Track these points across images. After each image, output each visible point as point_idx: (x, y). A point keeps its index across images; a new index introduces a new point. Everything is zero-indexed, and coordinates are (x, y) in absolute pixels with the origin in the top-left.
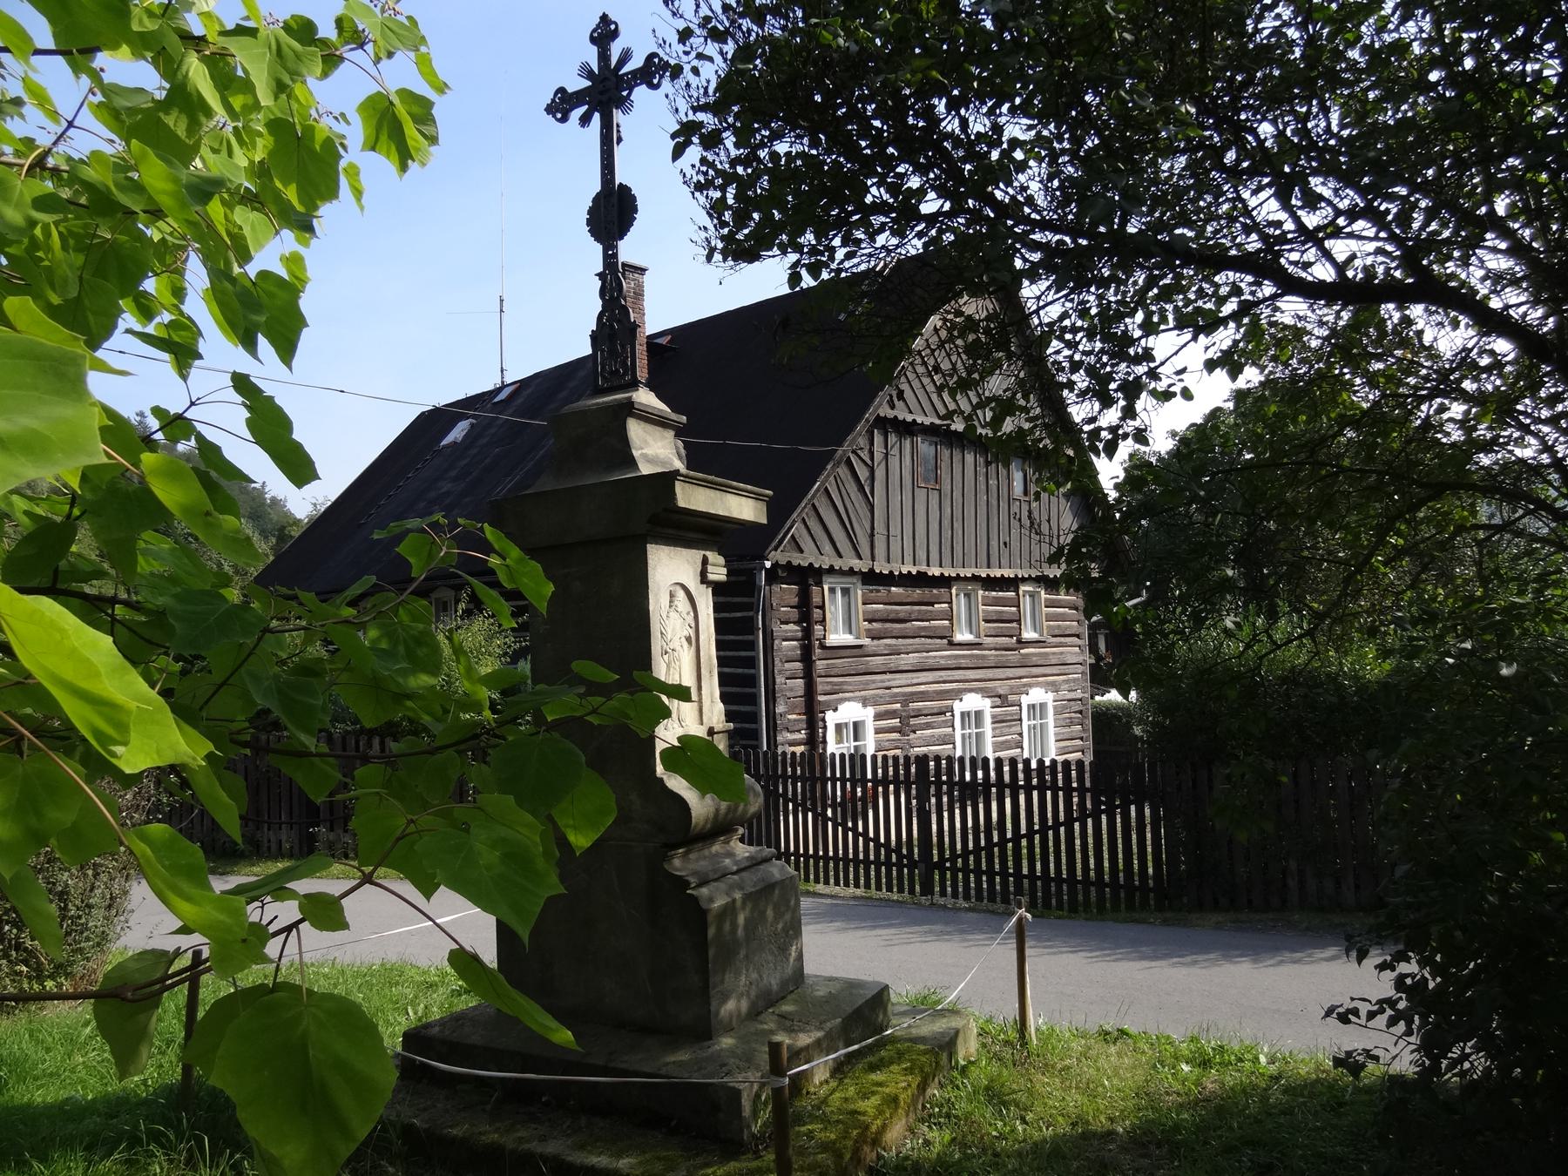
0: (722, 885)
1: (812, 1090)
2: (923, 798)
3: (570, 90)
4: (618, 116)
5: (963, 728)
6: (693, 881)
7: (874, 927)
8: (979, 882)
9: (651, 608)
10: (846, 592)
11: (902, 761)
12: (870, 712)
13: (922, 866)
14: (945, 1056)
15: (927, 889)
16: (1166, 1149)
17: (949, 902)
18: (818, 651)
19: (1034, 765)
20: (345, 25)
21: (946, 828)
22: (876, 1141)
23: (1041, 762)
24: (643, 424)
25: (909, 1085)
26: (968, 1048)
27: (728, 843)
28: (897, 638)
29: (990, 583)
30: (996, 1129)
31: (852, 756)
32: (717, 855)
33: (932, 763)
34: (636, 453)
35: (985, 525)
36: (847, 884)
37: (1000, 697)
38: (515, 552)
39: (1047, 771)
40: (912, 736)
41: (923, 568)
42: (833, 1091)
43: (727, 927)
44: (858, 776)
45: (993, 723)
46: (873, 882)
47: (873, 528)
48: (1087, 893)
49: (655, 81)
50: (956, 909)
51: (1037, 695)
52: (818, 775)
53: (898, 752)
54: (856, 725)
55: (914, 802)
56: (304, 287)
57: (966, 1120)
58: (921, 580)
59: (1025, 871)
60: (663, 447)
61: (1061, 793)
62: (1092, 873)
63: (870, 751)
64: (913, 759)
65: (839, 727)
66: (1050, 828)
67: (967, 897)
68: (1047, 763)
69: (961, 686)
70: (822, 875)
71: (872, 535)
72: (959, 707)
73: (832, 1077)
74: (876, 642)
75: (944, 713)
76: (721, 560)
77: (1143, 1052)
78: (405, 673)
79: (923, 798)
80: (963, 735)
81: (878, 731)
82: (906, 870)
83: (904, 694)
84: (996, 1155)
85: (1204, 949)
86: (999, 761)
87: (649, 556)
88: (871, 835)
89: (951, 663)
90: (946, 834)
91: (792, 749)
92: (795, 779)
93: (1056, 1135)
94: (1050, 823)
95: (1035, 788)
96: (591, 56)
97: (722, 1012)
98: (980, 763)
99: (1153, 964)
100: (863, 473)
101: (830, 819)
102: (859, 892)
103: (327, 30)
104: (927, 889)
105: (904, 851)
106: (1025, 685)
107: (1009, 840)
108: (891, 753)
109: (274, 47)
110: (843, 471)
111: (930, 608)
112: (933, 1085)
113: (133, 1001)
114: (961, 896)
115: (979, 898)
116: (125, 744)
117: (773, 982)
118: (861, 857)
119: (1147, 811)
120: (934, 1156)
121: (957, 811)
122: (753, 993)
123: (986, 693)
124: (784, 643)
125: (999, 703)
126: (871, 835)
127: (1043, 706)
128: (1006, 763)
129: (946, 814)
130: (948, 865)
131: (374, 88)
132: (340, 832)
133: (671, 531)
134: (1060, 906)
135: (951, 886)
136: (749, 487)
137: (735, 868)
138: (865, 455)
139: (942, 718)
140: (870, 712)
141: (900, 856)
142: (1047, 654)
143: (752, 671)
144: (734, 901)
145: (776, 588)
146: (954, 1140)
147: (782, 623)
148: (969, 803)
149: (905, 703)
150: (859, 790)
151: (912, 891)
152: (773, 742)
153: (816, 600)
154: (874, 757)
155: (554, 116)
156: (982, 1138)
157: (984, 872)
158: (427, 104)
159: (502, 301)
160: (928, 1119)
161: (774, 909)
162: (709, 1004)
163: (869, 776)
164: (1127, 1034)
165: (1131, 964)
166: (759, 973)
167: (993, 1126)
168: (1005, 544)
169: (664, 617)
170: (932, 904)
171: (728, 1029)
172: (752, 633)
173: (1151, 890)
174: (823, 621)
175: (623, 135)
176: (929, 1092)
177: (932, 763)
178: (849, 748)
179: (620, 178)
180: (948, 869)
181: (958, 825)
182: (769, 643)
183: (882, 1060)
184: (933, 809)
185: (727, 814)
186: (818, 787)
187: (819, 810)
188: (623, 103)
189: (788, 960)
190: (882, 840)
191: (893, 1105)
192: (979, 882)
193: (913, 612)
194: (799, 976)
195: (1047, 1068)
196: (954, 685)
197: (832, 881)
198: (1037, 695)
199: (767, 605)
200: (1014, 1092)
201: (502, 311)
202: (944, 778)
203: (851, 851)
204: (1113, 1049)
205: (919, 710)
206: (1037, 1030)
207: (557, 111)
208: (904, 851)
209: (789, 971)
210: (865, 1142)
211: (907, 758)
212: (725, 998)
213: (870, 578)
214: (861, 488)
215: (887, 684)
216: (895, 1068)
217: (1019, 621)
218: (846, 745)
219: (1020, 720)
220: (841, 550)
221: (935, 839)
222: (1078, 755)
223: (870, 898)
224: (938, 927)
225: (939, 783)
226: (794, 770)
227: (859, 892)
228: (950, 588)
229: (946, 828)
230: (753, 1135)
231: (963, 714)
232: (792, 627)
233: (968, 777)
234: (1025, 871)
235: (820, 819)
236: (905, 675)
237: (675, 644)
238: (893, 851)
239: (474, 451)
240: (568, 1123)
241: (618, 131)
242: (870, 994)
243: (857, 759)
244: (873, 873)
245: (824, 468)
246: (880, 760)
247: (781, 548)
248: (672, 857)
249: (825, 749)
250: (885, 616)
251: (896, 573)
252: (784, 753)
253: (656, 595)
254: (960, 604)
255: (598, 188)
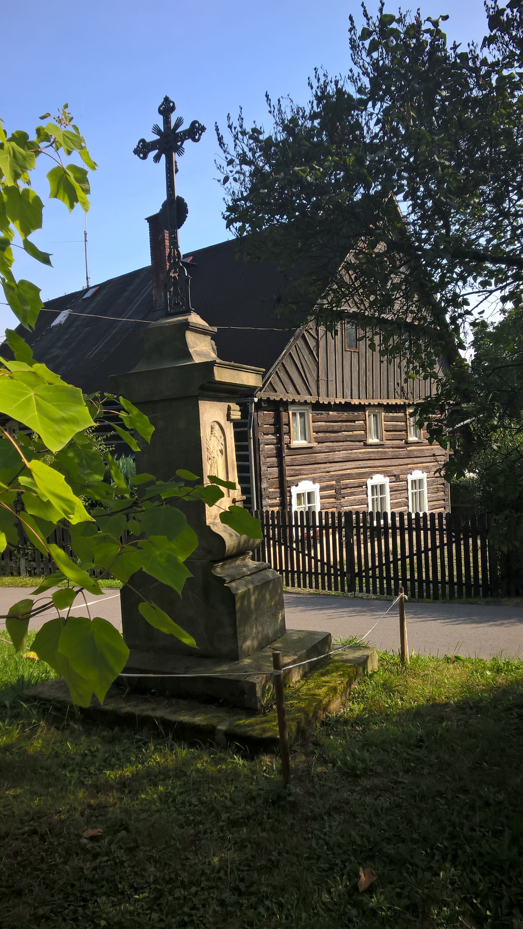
0: (242, 581)
1: (292, 685)
2: (349, 536)
3: (148, 140)
4: (176, 157)
5: (373, 495)
6: (228, 579)
7: (322, 609)
8: (381, 584)
9: (202, 435)
10: (302, 415)
11: (336, 515)
12: (317, 486)
13: (349, 575)
14: (361, 669)
15: (352, 588)
16: (474, 710)
17: (364, 595)
18: (286, 451)
19: (413, 516)
20: (41, 132)
21: (363, 553)
22: (325, 709)
23: (417, 514)
24: (194, 334)
25: (342, 682)
26: (373, 665)
27: (244, 560)
28: (333, 442)
29: (389, 408)
30: (387, 703)
31: (307, 513)
32: (239, 566)
33: (354, 516)
34: (191, 350)
35: (385, 374)
36: (305, 586)
37: (395, 476)
38: (135, 411)
39: (422, 520)
40: (343, 500)
41: (348, 400)
42: (303, 685)
43: (246, 603)
44: (311, 524)
45: (391, 491)
46: (320, 585)
47: (318, 376)
48: (444, 588)
49: (197, 137)
50: (368, 599)
51: (417, 475)
52: (287, 524)
53: (334, 510)
54: (309, 494)
55: (344, 539)
56: (11, 264)
57: (372, 700)
58: (347, 407)
59: (408, 577)
60: (205, 346)
61: (429, 532)
62: (447, 578)
63: (318, 510)
64: (343, 514)
65: (299, 496)
66: (423, 552)
67: (375, 592)
68: (421, 515)
69: (371, 470)
70: (290, 581)
71: (318, 381)
72: (370, 482)
73: (301, 679)
74: (321, 445)
75: (362, 486)
76: (238, 408)
77: (468, 667)
78: (90, 474)
79: (349, 536)
80: (373, 499)
81: (322, 498)
82: (339, 578)
83: (337, 475)
84: (387, 715)
85: (508, 616)
86: (393, 514)
87: (200, 407)
88: (319, 558)
89: (366, 456)
90: (363, 557)
91: (272, 509)
92: (274, 526)
93: (419, 705)
94: (423, 549)
95: (414, 529)
96: (159, 121)
97: (244, 646)
98: (382, 516)
99: (479, 625)
100: (312, 343)
101: (295, 549)
102: (312, 591)
103: (33, 137)
104: (352, 588)
105: (338, 567)
106: (410, 469)
107: (399, 560)
108: (330, 510)
109: (12, 153)
110: (300, 343)
111: (353, 424)
112: (354, 683)
113: (22, 620)
114: (371, 592)
115: (382, 593)
116: (73, 514)
117: (269, 632)
118: (313, 571)
119: (479, 542)
120: (355, 716)
121: (369, 544)
122: (260, 637)
123: (386, 474)
124: (266, 446)
125: (394, 480)
126: (319, 558)
127: (421, 481)
128: (397, 515)
129: (362, 546)
130: (364, 574)
131: (55, 165)
132: (8, 560)
133: (211, 393)
134: (428, 596)
135: (366, 586)
136: (253, 367)
137: (249, 573)
138: (313, 333)
139: (360, 489)
140: (317, 486)
141: (336, 570)
142: (423, 450)
143: (247, 463)
144: (249, 589)
145: (260, 413)
146: (364, 709)
147: (265, 434)
148: (376, 539)
149: (338, 481)
150: (311, 532)
151: (343, 590)
152: (260, 505)
153: (285, 420)
154: (320, 513)
155: (139, 156)
156: (380, 707)
157: (384, 578)
158: (85, 173)
159: (86, 234)
160: (352, 699)
161: (270, 594)
162: (237, 643)
163: (318, 524)
164: (460, 659)
165: (466, 625)
166: (262, 627)
167: (385, 701)
168: (398, 384)
169: (208, 439)
170: (355, 597)
171: (248, 656)
172: (247, 441)
173: (480, 586)
174: (289, 433)
175: (178, 168)
176: (353, 686)
177: (354, 516)
178: (305, 508)
179: (178, 193)
180: (364, 576)
181: (369, 552)
182: (257, 446)
183: (328, 671)
184: (355, 543)
185: (244, 544)
186: (288, 530)
187: (288, 544)
188: (179, 150)
189: (277, 621)
190: (325, 561)
191: (333, 692)
192: (381, 584)
193: (343, 426)
194: (283, 628)
195: (416, 675)
196: (367, 470)
197: (296, 585)
198: (417, 475)
199: (256, 424)
200: (397, 686)
201: (86, 240)
202: (361, 525)
203: (307, 568)
204: (451, 666)
205: (347, 484)
206: (411, 657)
207: (140, 153)
208: (338, 567)
209: (278, 627)
210: (320, 708)
211: (340, 513)
212: (245, 639)
213: (317, 407)
214: (311, 352)
215: (327, 470)
216: (334, 674)
217: (406, 431)
218: (304, 506)
219: (407, 489)
220: (299, 390)
221: (356, 560)
222: (439, 510)
223: (319, 594)
224: (358, 608)
225: (358, 528)
226: (273, 522)
227: (312, 591)
228: (365, 411)
229: (363, 553)
230: (262, 706)
231: (372, 487)
232: (270, 436)
233: (375, 524)
234: (408, 577)
235: (289, 549)
236: (338, 464)
237: (215, 454)
238: (332, 567)
239: (72, 329)
240: (166, 703)
241: (176, 166)
242: (321, 638)
243: (310, 513)
244: (320, 580)
245: (288, 341)
246: (323, 515)
247: (264, 390)
248: (216, 567)
249: (291, 509)
250: (326, 429)
251: (333, 403)
252: (267, 512)
253: (204, 428)
254: (371, 421)
255: (165, 198)
